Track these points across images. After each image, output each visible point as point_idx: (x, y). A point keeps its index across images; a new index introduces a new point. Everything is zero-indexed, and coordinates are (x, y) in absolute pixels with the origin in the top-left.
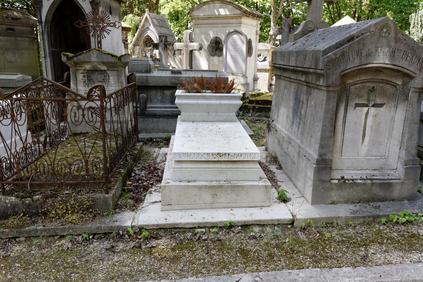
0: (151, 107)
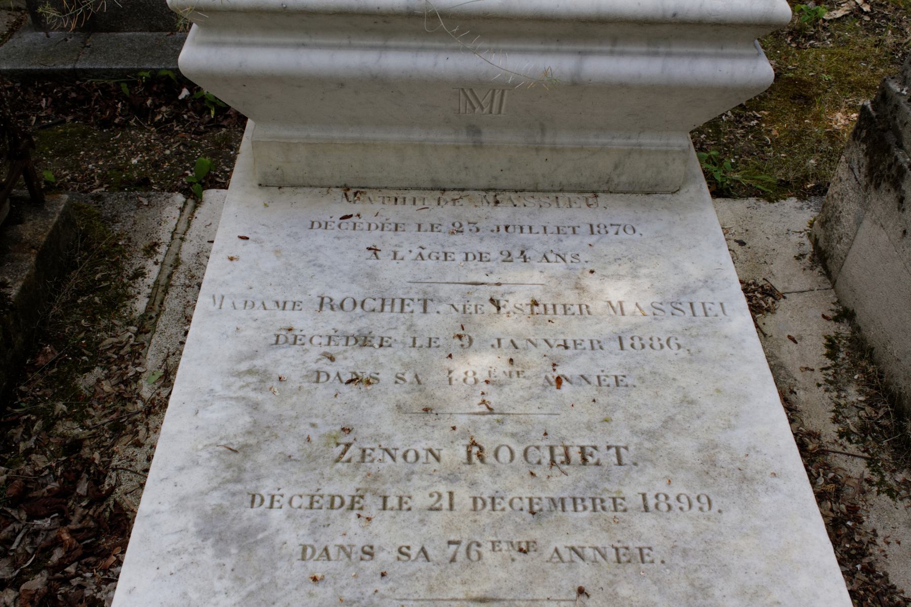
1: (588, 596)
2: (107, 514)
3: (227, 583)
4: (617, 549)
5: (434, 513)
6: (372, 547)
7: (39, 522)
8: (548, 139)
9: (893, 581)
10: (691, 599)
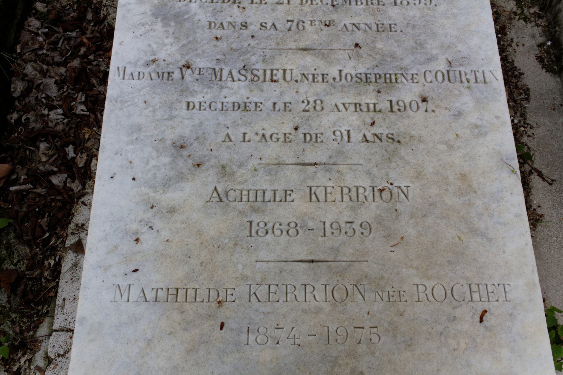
1: (360, 48)
2: (105, 30)
3: (171, 40)
4: (377, 25)
5: (279, 6)
6: (246, 23)
7: (70, 33)
9: (516, 64)
10: (414, 50)
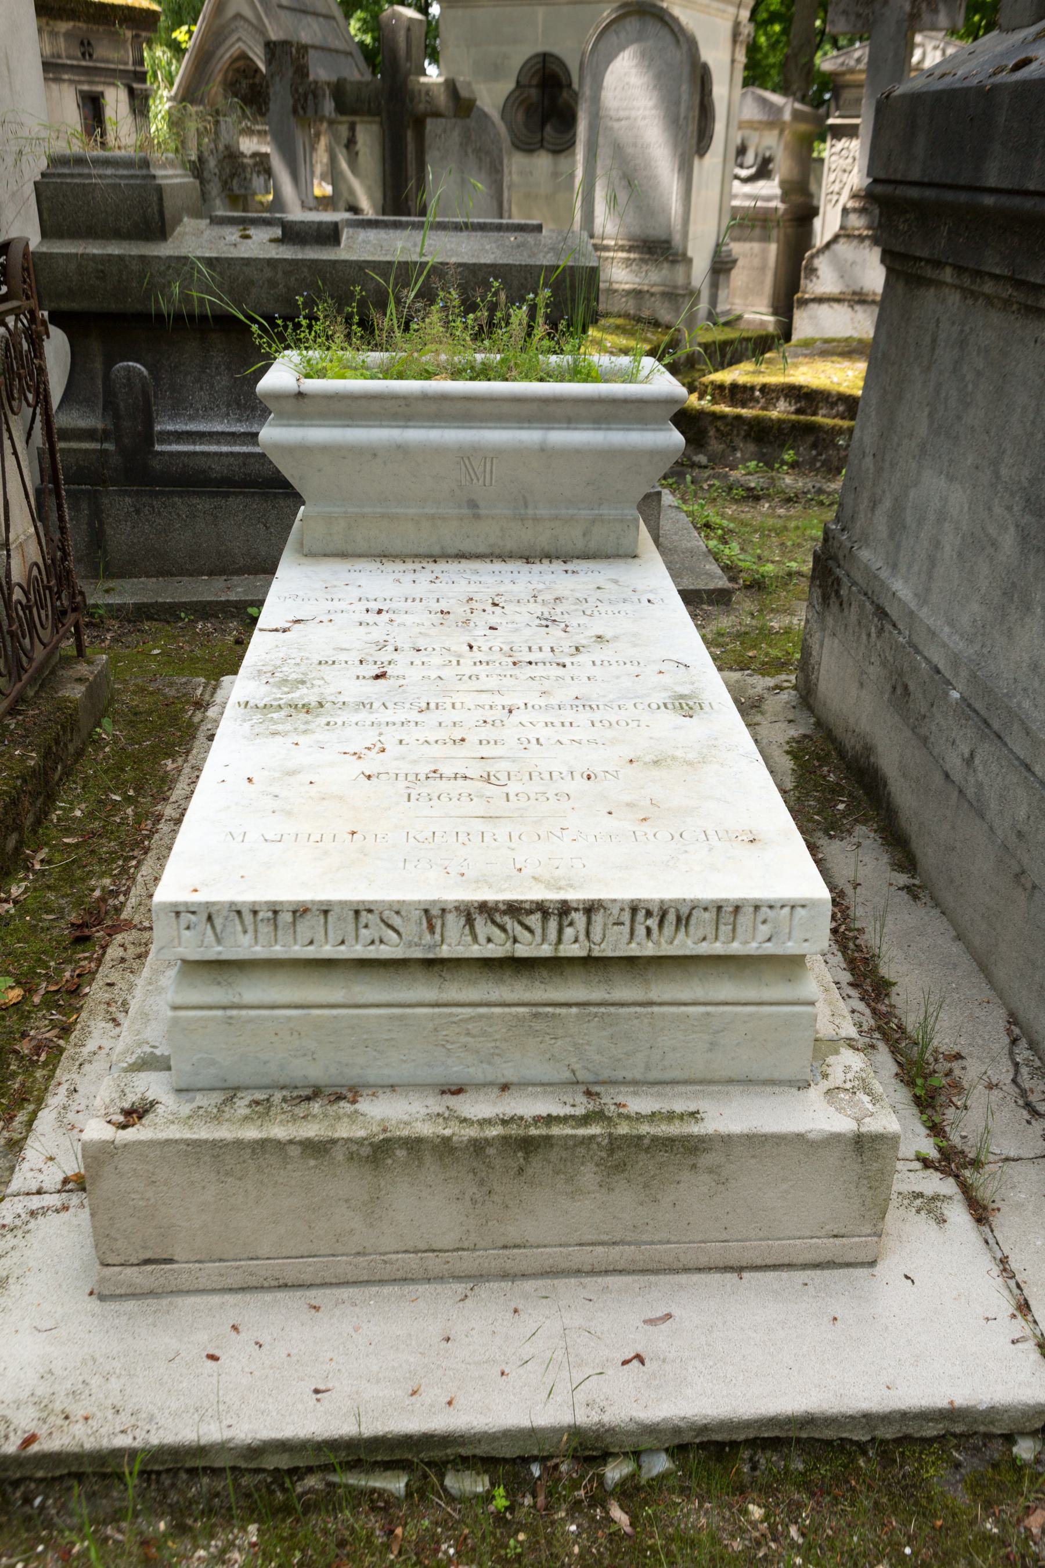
0: (180, 437)
8: (530, 512)
